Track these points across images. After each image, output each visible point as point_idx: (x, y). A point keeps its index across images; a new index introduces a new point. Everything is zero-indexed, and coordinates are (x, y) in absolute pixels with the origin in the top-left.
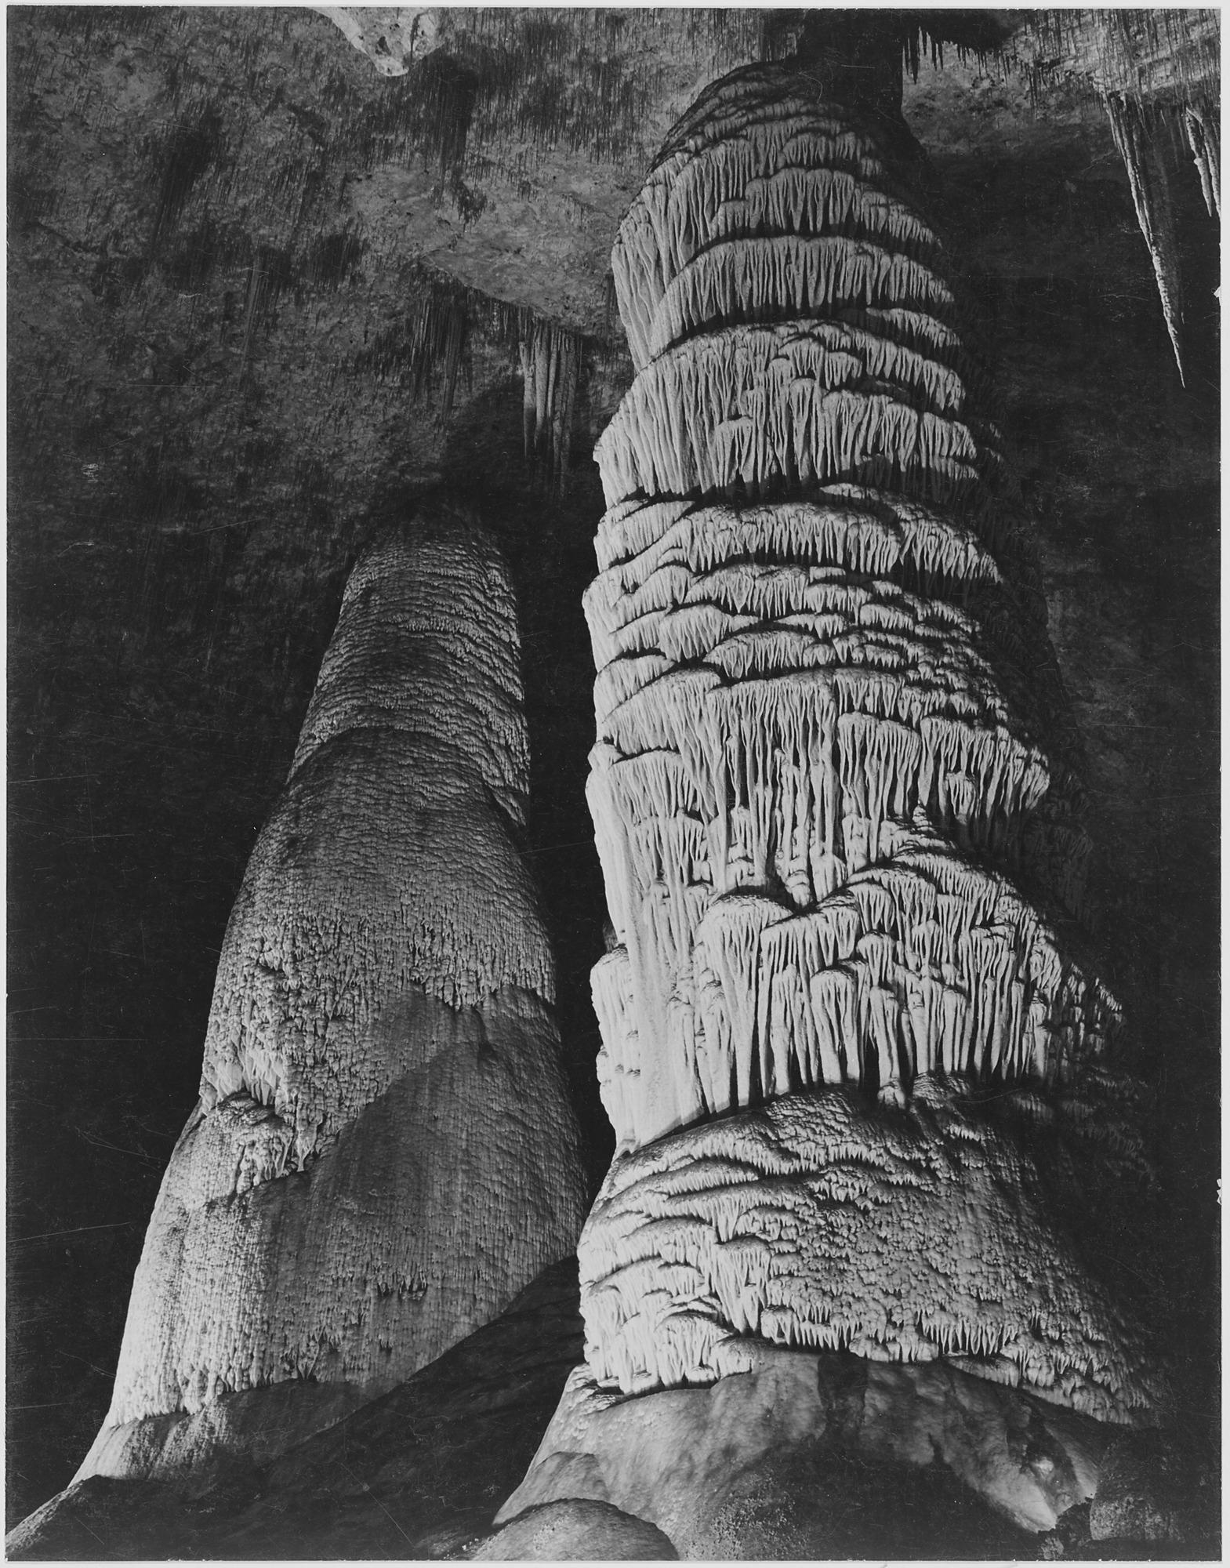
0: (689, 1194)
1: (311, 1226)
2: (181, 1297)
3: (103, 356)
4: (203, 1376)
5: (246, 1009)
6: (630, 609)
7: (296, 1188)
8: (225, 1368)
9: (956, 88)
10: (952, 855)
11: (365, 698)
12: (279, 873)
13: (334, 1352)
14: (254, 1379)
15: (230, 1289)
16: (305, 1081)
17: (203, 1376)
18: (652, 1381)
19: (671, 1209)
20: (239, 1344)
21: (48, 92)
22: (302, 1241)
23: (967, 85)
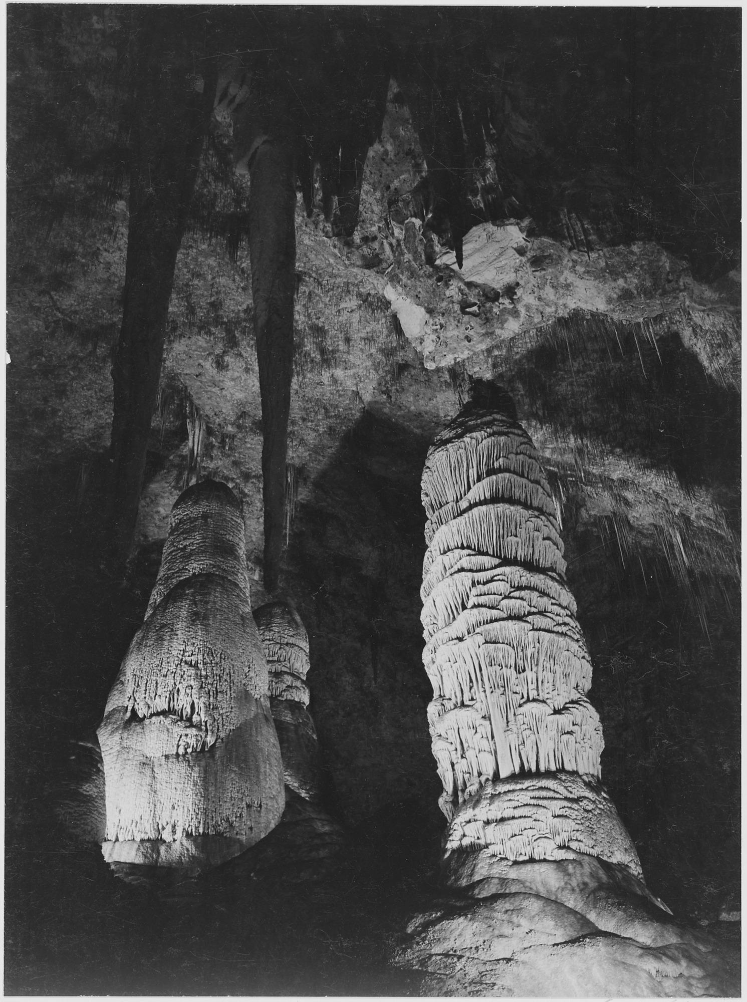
0: (539, 798)
1: (219, 774)
3: (27, 353)
4: (174, 827)
5: (178, 679)
14: (201, 831)
16: (210, 715)
17: (174, 827)
18: (527, 858)
20: (194, 817)
22: (216, 780)
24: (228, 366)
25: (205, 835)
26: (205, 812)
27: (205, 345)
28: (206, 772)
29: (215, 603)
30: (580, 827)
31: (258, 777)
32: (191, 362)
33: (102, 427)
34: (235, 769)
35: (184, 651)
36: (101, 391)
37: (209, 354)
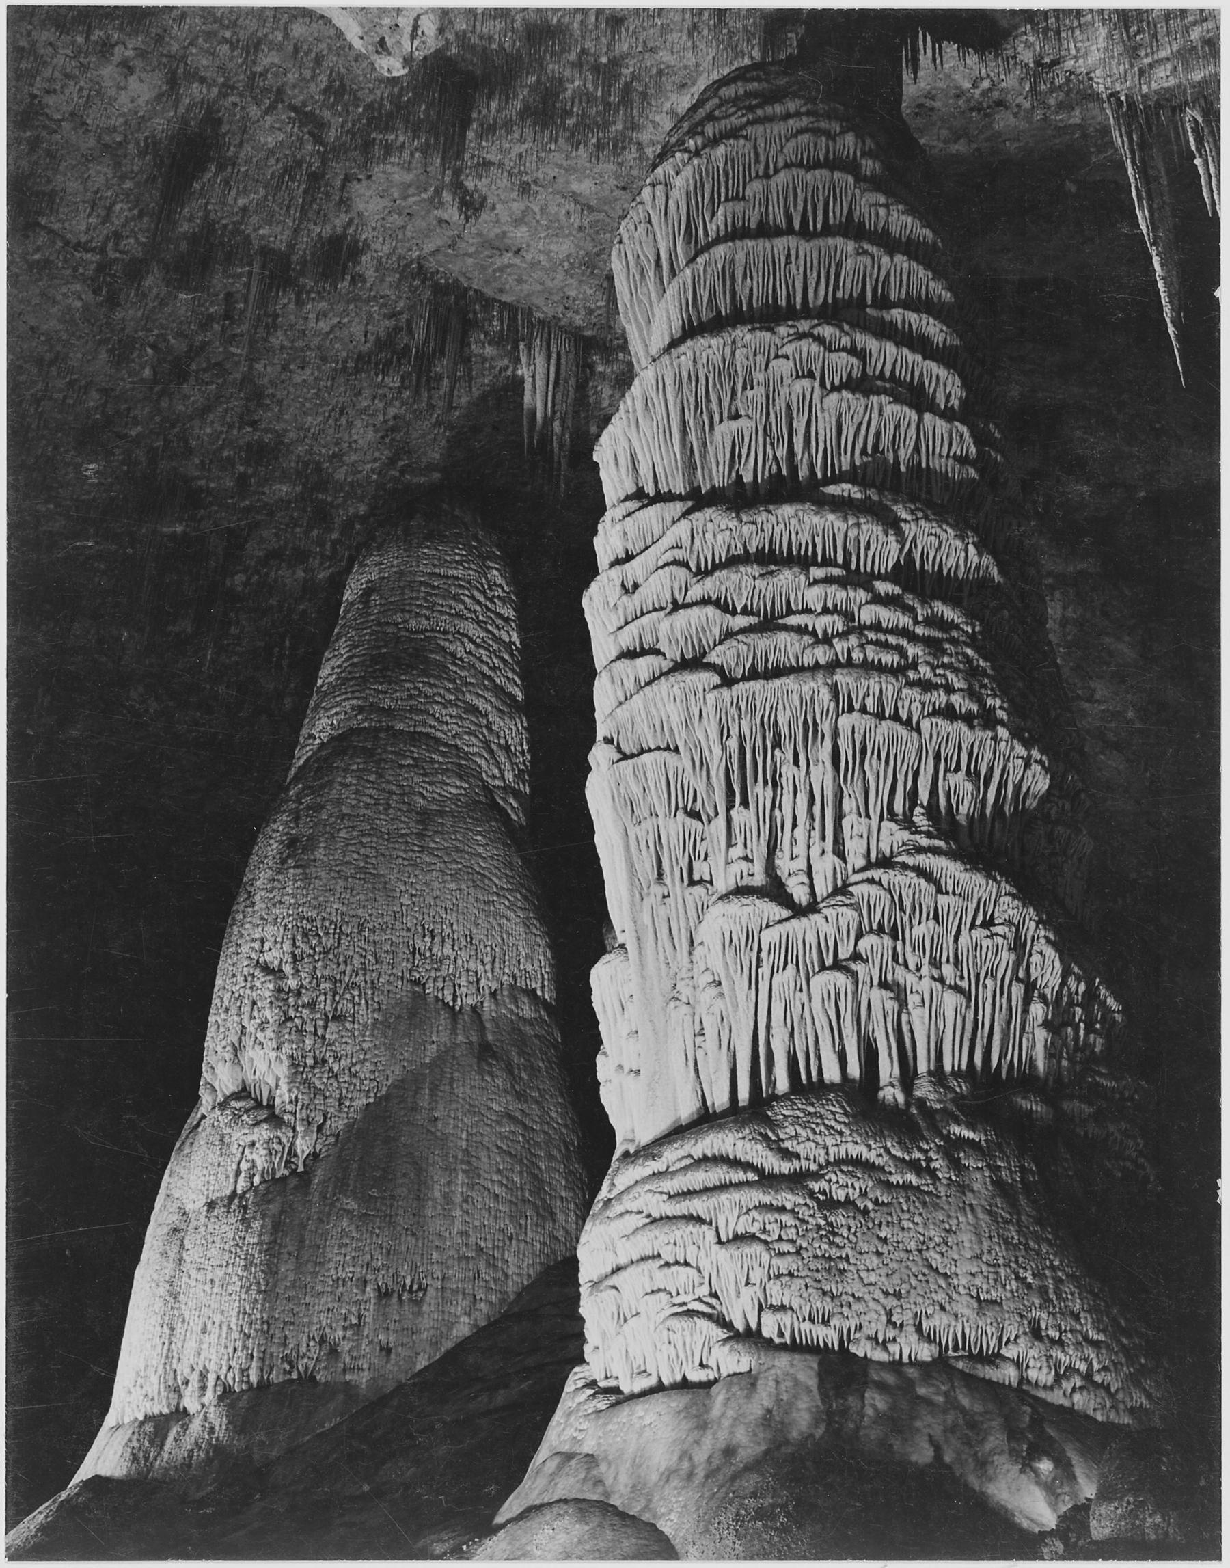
0: (689, 1194)
1: (311, 1226)
3: (103, 356)
4: (203, 1376)
6: (630, 609)
7: (296, 1187)
8: (225, 1368)
9: (956, 88)
10: (952, 855)
12: (279, 873)
13: (334, 1352)
14: (254, 1378)
15: (230, 1288)
16: (305, 1081)
19: (671, 1209)
20: (239, 1344)
21: (48, 92)
22: (302, 1241)
23: (967, 85)
25: (263, 1386)
26: (267, 1329)
28: (277, 1227)
31: (418, 1214)
32: (421, 223)
34: (352, 1205)
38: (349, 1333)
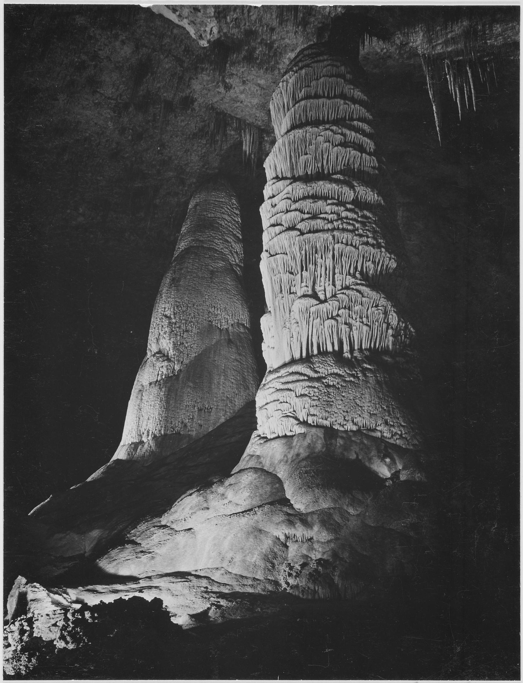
2: (142, 409)
4: (148, 432)
11: (195, 237)
12: (170, 288)
13: (185, 426)
14: (162, 433)
16: (178, 349)
17: (148, 432)
18: (277, 435)
20: (158, 423)
21: (100, 50)
24: (232, 85)
27: (209, 78)
29: (187, 268)
30: (317, 403)
31: (210, 387)
33: (204, 156)
34: (191, 385)
35: (165, 308)
36: (183, 134)
37: (218, 83)
38: (190, 420)
